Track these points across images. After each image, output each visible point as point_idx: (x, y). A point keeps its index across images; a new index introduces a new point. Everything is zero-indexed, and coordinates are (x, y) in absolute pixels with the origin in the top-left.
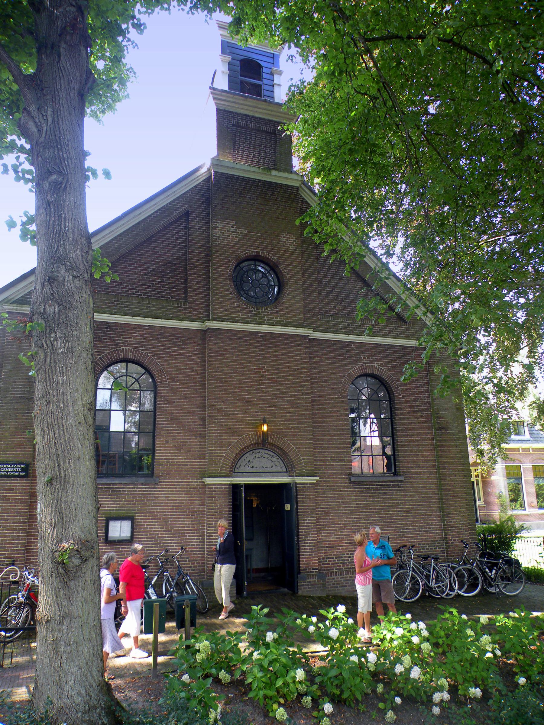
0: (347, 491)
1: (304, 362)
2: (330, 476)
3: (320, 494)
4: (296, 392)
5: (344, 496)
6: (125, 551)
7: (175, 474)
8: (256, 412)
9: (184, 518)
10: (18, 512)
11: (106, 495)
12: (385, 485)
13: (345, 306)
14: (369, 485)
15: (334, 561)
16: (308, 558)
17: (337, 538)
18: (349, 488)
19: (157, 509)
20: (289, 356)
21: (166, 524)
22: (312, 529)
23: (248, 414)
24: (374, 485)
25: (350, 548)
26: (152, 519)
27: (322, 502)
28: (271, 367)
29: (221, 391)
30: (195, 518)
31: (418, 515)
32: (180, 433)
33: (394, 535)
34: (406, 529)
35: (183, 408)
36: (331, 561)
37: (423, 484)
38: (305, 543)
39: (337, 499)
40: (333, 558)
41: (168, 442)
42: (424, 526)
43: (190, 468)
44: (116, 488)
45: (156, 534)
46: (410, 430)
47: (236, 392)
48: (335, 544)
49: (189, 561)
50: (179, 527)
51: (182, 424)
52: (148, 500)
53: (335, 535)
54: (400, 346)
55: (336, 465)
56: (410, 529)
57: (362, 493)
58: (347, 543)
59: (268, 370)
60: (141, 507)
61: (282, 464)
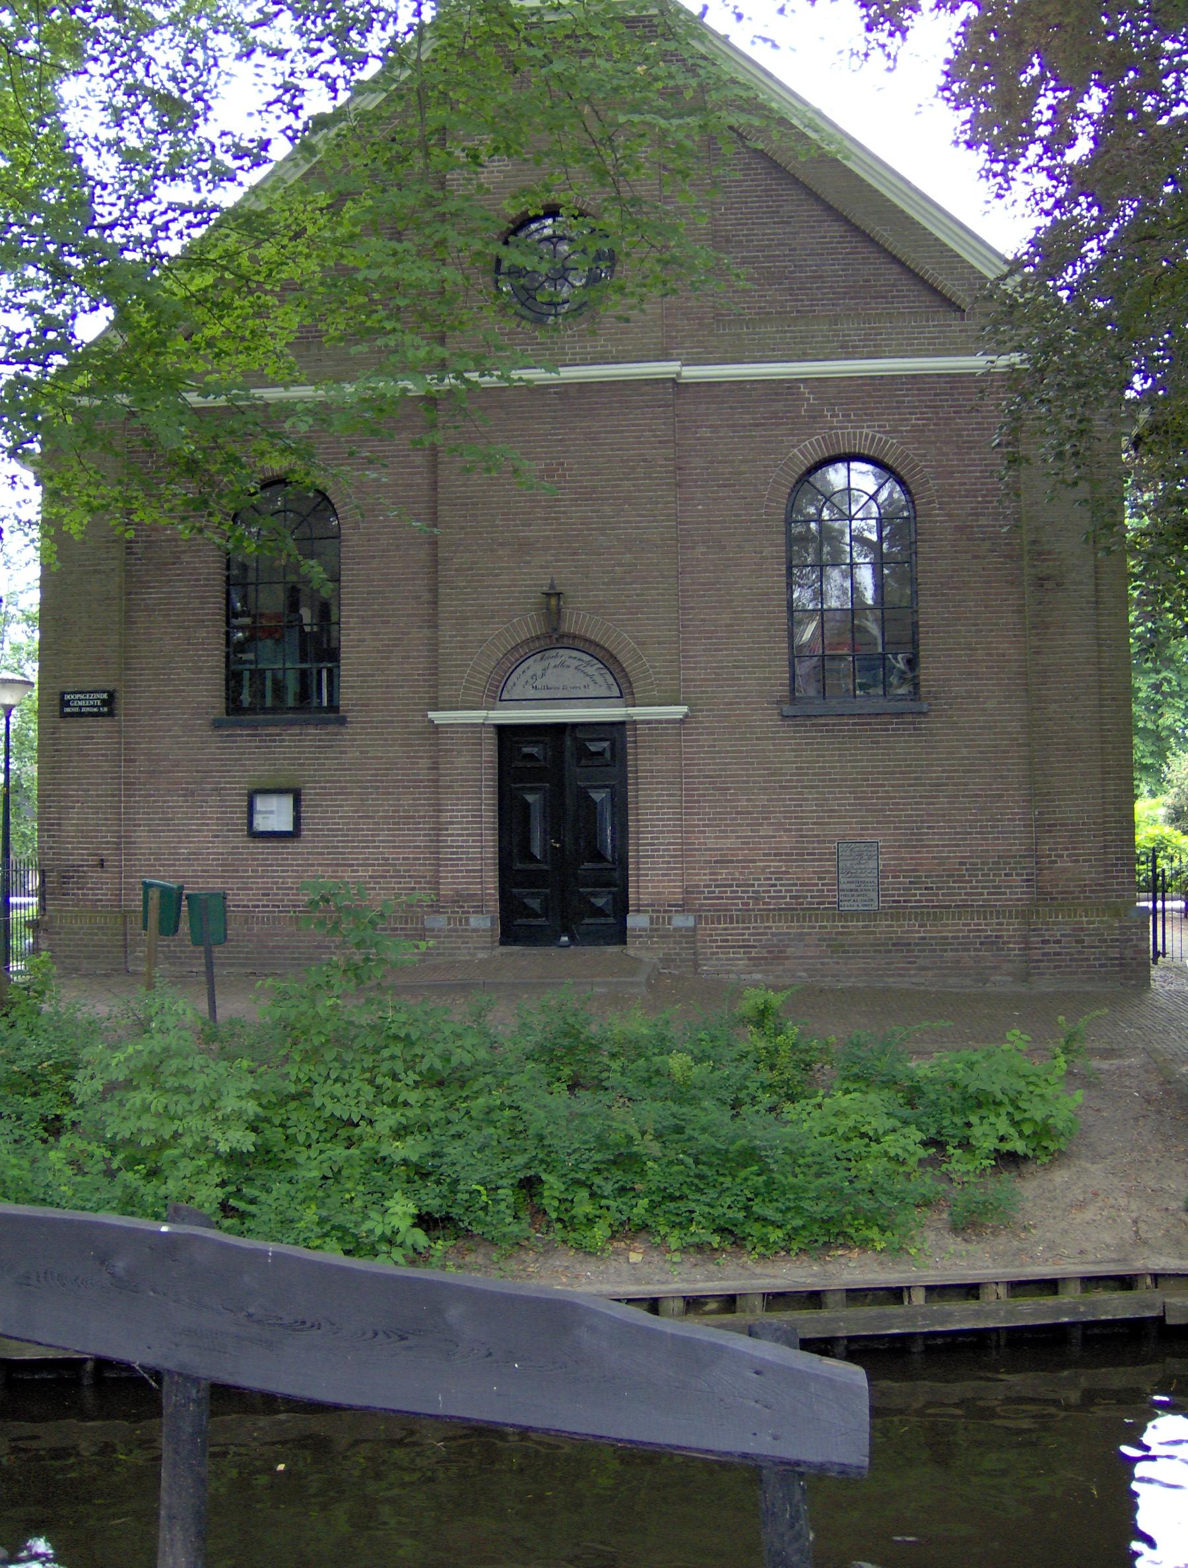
0: (773, 738)
1: (660, 442)
2: (731, 704)
3: (703, 746)
4: (639, 516)
5: (763, 751)
6: (289, 853)
7: (378, 705)
8: (542, 567)
9: (399, 794)
10: (103, 778)
11: (250, 747)
12: (876, 724)
13: (792, 289)
14: (834, 725)
15: (732, 892)
16: (659, 881)
17: (743, 843)
18: (778, 732)
19: (345, 776)
20: (623, 431)
21: (364, 805)
22: (669, 819)
23: (525, 574)
24: (847, 724)
25: (775, 867)
26: (336, 794)
27: (709, 764)
28: (578, 463)
29: (463, 528)
30: (420, 793)
31: (963, 796)
32: (388, 622)
33: (895, 841)
34: (928, 828)
35: (393, 568)
36: (726, 892)
37: (985, 721)
38: (652, 850)
39: (747, 757)
40: (731, 886)
41: (364, 640)
42: (979, 821)
43: (409, 692)
44: (267, 735)
45: (344, 824)
46: (956, 588)
47: (497, 526)
48: (737, 855)
49: (410, 877)
50: (388, 811)
51: (392, 603)
52: (327, 758)
53: (738, 837)
54: (939, 375)
55: (746, 679)
56: (938, 827)
57: (812, 744)
58: (770, 855)
59: (571, 470)
60: (315, 770)
61: (611, 680)
